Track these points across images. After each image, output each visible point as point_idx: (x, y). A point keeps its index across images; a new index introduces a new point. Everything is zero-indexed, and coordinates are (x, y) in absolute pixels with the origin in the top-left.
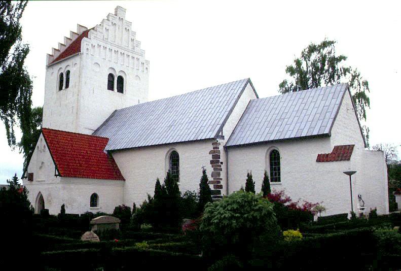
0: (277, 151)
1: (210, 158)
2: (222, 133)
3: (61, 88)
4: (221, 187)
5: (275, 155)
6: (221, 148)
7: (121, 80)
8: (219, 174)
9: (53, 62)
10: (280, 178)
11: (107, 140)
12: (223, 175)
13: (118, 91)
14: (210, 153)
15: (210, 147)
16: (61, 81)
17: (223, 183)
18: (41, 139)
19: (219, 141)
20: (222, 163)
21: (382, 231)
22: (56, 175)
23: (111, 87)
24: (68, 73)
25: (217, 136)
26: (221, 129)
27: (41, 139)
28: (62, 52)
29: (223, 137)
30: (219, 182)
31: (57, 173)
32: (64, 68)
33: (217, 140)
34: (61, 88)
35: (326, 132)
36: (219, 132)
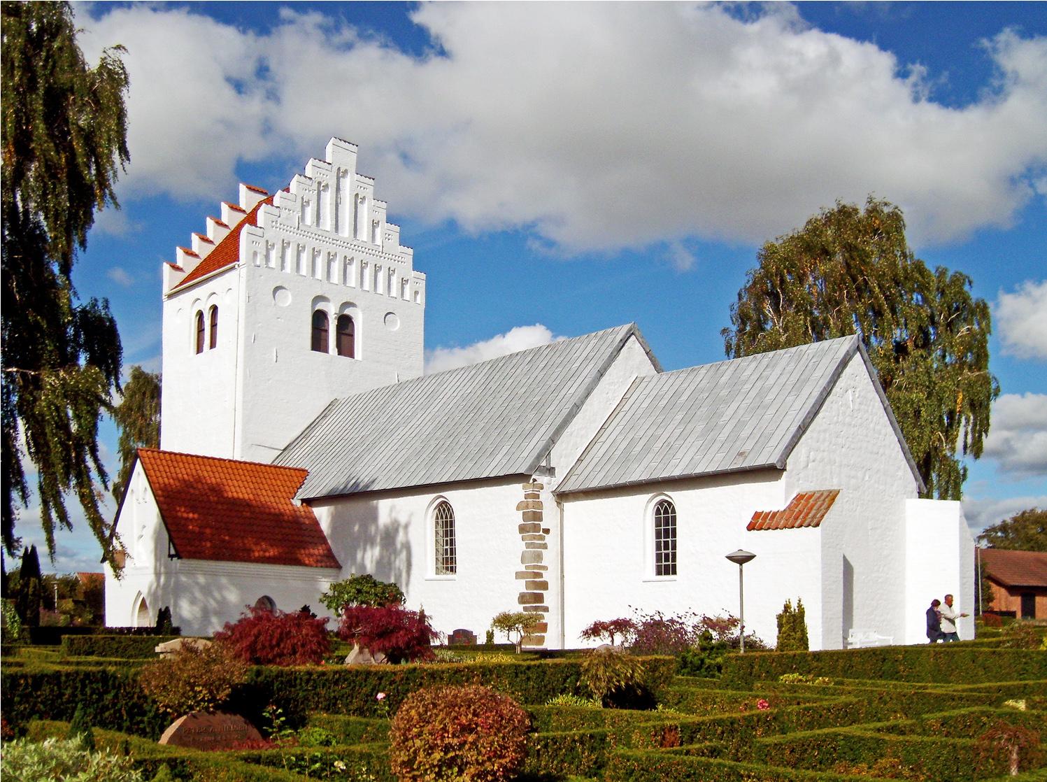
0: (670, 504)
1: (518, 519)
2: (549, 461)
3: (199, 349)
4: (544, 586)
5: (666, 511)
6: (547, 498)
7: (345, 323)
8: (539, 557)
9: (181, 284)
10: (674, 567)
11: (303, 474)
12: (549, 558)
13: (340, 353)
14: (518, 508)
15: (517, 491)
16: (201, 330)
17: (549, 576)
18: (139, 474)
19: (543, 479)
20: (547, 531)
21: (67, 696)
22: (171, 556)
23: (318, 343)
24: (215, 309)
25: (535, 467)
26: (546, 451)
27: (139, 474)
28: (217, 244)
29: (551, 471)
30: (540, 575)
31: (173, 552)
32: (204, 299)
33: (533, 477)
34: (199, 349)
35: (773, 459)
36: (539, 457)
